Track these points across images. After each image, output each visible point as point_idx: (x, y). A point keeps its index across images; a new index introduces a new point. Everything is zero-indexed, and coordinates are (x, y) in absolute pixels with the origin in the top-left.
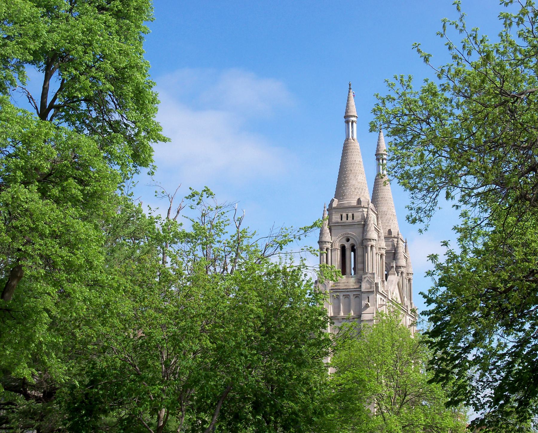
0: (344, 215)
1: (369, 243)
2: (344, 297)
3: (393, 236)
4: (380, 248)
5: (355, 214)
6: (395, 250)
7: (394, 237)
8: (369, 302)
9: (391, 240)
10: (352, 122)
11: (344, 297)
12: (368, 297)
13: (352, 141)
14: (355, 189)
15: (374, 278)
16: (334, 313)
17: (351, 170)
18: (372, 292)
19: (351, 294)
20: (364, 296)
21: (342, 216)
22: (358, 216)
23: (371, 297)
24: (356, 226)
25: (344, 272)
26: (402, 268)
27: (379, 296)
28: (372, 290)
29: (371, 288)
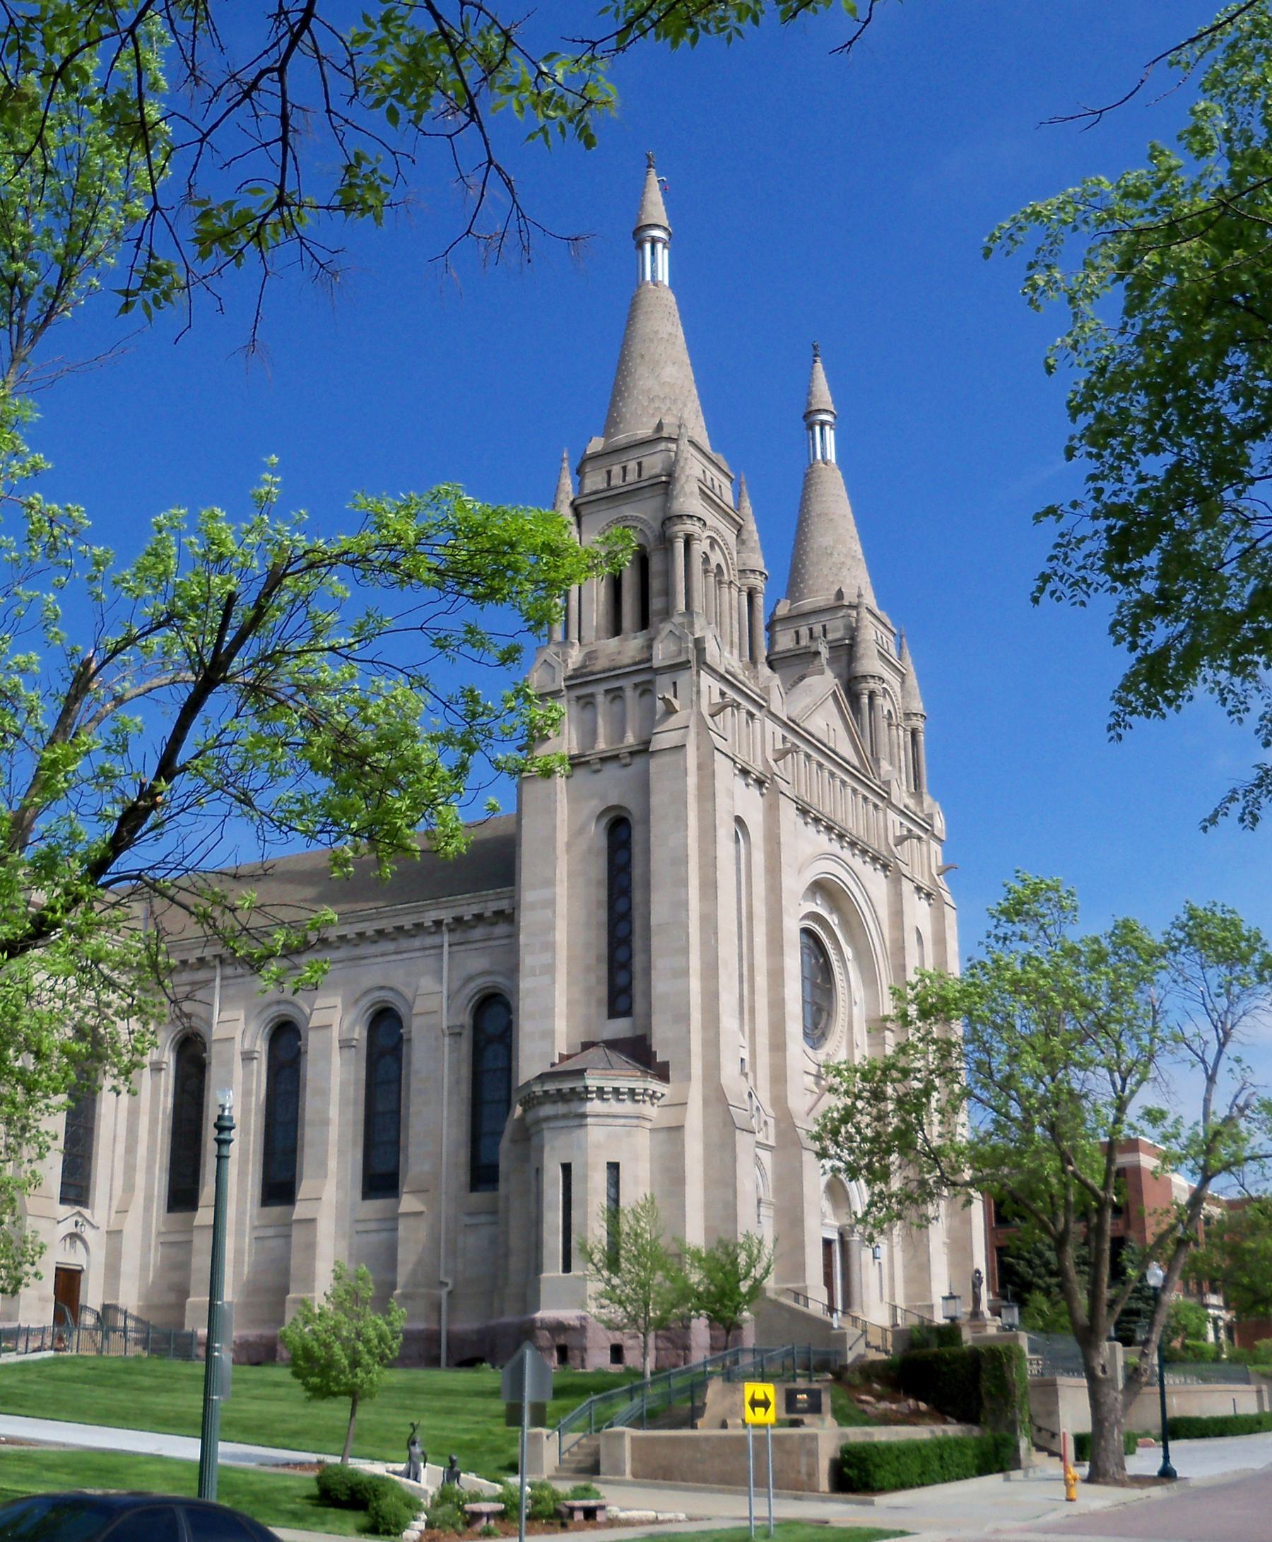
0: (804, 631)
1: (864, 685)
2: (610, 697)
3: (846, 603)
4: (742, 571)
5: (646, 462)
6: (853, 638)
7: (851, 607)
8: (675, 697)
9: (841, 614)
10: (654, 241)
11: (610, 697)
12: (675, 684)
13: (652, 287)
14: (651, 400)
15: (691, 625)
16: (581, 742)
17: (642, 356)
18: (684, 665)
19: (627, 683)
20: (663, 682)
21: (797, 633)
22: (654, 463)
23: (683, 679)
24: (647, 493)
25: (616, 630)
26: (871, 681)
27: (706, 680)
28: (682, 659)
29: (680, 653)
